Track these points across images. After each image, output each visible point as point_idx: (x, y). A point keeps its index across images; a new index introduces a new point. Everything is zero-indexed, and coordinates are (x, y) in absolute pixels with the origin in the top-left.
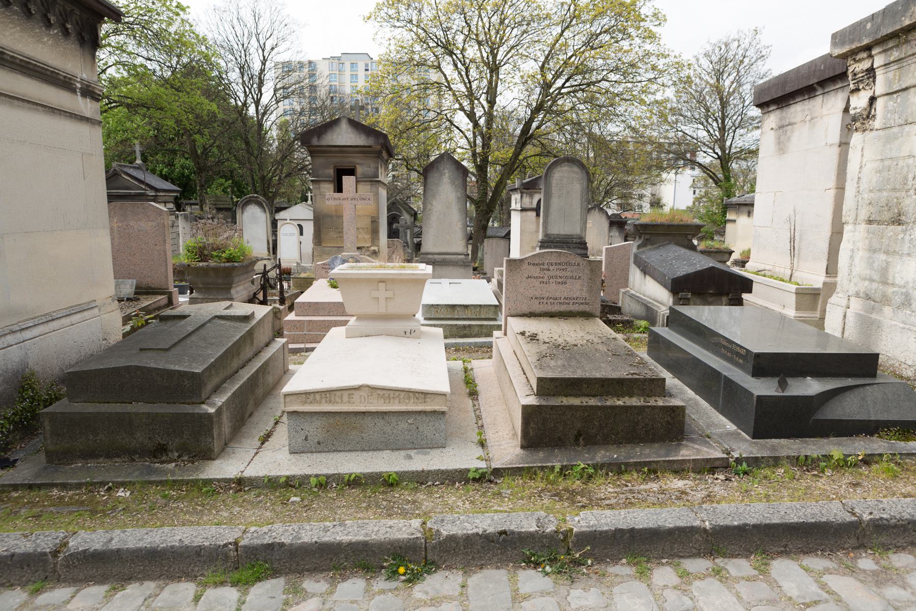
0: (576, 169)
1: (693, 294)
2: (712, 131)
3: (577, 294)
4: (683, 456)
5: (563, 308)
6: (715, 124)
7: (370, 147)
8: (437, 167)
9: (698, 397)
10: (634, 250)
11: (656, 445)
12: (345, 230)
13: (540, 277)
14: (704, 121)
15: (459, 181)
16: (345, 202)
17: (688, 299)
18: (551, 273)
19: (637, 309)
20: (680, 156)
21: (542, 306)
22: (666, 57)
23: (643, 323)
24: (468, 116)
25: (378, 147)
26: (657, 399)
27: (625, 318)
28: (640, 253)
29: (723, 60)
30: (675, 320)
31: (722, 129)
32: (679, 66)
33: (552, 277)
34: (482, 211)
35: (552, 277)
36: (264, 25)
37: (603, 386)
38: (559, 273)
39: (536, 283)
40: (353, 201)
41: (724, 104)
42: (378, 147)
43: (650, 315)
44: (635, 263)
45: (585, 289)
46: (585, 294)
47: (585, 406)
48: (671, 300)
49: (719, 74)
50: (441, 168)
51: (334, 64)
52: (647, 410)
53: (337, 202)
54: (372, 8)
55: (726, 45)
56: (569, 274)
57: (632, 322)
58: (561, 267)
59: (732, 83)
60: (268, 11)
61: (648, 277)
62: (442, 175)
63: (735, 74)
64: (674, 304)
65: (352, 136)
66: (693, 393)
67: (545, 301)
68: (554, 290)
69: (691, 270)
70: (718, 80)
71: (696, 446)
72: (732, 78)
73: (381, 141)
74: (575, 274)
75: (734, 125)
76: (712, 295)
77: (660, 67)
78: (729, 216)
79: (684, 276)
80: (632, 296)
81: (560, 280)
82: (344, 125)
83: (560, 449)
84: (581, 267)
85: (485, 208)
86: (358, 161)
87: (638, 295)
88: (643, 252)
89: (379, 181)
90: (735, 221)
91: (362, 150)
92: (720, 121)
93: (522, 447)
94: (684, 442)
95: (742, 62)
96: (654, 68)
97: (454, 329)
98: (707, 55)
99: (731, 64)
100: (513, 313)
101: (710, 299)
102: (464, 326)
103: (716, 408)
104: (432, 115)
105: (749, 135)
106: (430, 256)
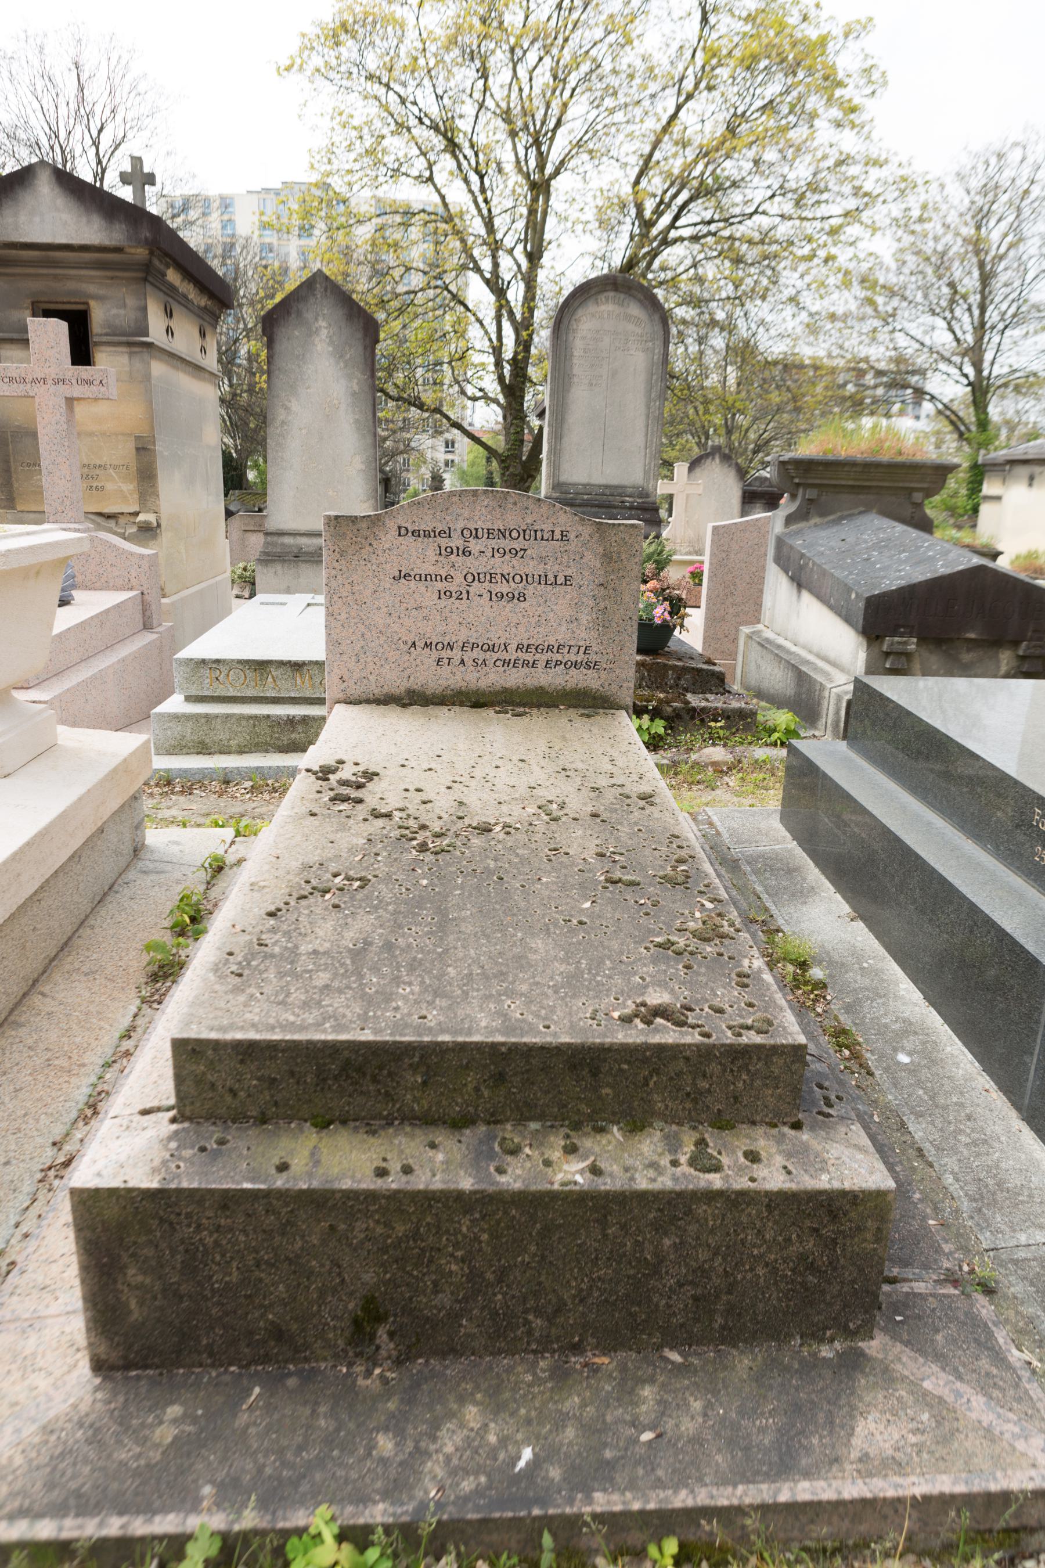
0: (635, 310)
1: (922, 640)
2: (959, 334)
3: (561, 634)
4: (867, 1466)
5: (515, 679)
6: (966, 318)
7: (118, 250)
8: (299, 313)
9: (934, 1020)
10: (778, 527)
11: (743, 1363)
12: (44, 463)
13: (438, 577)
14: (947, 312)
15: (355, 351)
16: (38, 390)
17: (908, 655)
18: (475, 565)
19: (775, 678)
20: (897, 383)
21: (445, 670)
22: (878, 163)
23: (783, 718)
24: (487, 282)
25: (141, 253)
26: (762, 1141)
27: (735, 704)
28: (789, 535)
29: (991, 189)
30: (869, 719)
31: (980, 328)
32: (905, 185)
33: (477, 578)
34: (513, 475)
35: (477, 578)
36: (95, 92)
37: (500, 1078)
38: (501, 565)
39: (427, 595)
40: (61, 388)
41: (986, 279)
42: (141, 253)
43: (805, 703)
44: (778, 560)
45: (585, 618)
46: (584, 636)
47: (395, 1196)
48: (862, 656)
49: (981, 217)
50: (309, 316)
51: (268, 203)
52: (701, 1209)
53: (18, 389)
54: (293, 46)
55: (1000, 156)
56: (532, 568)
57: (753, 714)
58: (506, 544)
59: (1006, 235)
60: (104, 63)
61: (806, 595)
62: (311, 333)
63: (1011, 218)
64: (870, 671)
65: (66, 216)
66: (917, 996)
67: (456, 654)
68: (484, 618)
69: (920, 574)
70: (978, 228)
71: (936, 1381)
72: (1004, 225)
73: (146, 233)
74: (552, 568)
75: (1002, 319)
76: (974, 644)
77: (868, 187)
78: (988, 488)
79: (901, 590)
80: (765, 645)
81: (504, 588)
82: (45, 187)
83: (273, 1383)
84: (573, 545)
85: (519, 470)
86: (92, 289)
87: (780, 641)
88: (799, 532)
89: (150, 345)
90: (998, 498)
91: (100, 259)
92: (976, 312)
93: (99, 1366)
94: (875, 1346)
95: (1027, 192)
96: (857, 191)
97: (263, 729)
98: (960, 177)
99: (1004, 198)
100: (356, 691)
101: (966, 657)
102: (291, 721)
103: (1011, 1088)
104: (416, 280)
105: (1030, 341)
106: (288, 540)
